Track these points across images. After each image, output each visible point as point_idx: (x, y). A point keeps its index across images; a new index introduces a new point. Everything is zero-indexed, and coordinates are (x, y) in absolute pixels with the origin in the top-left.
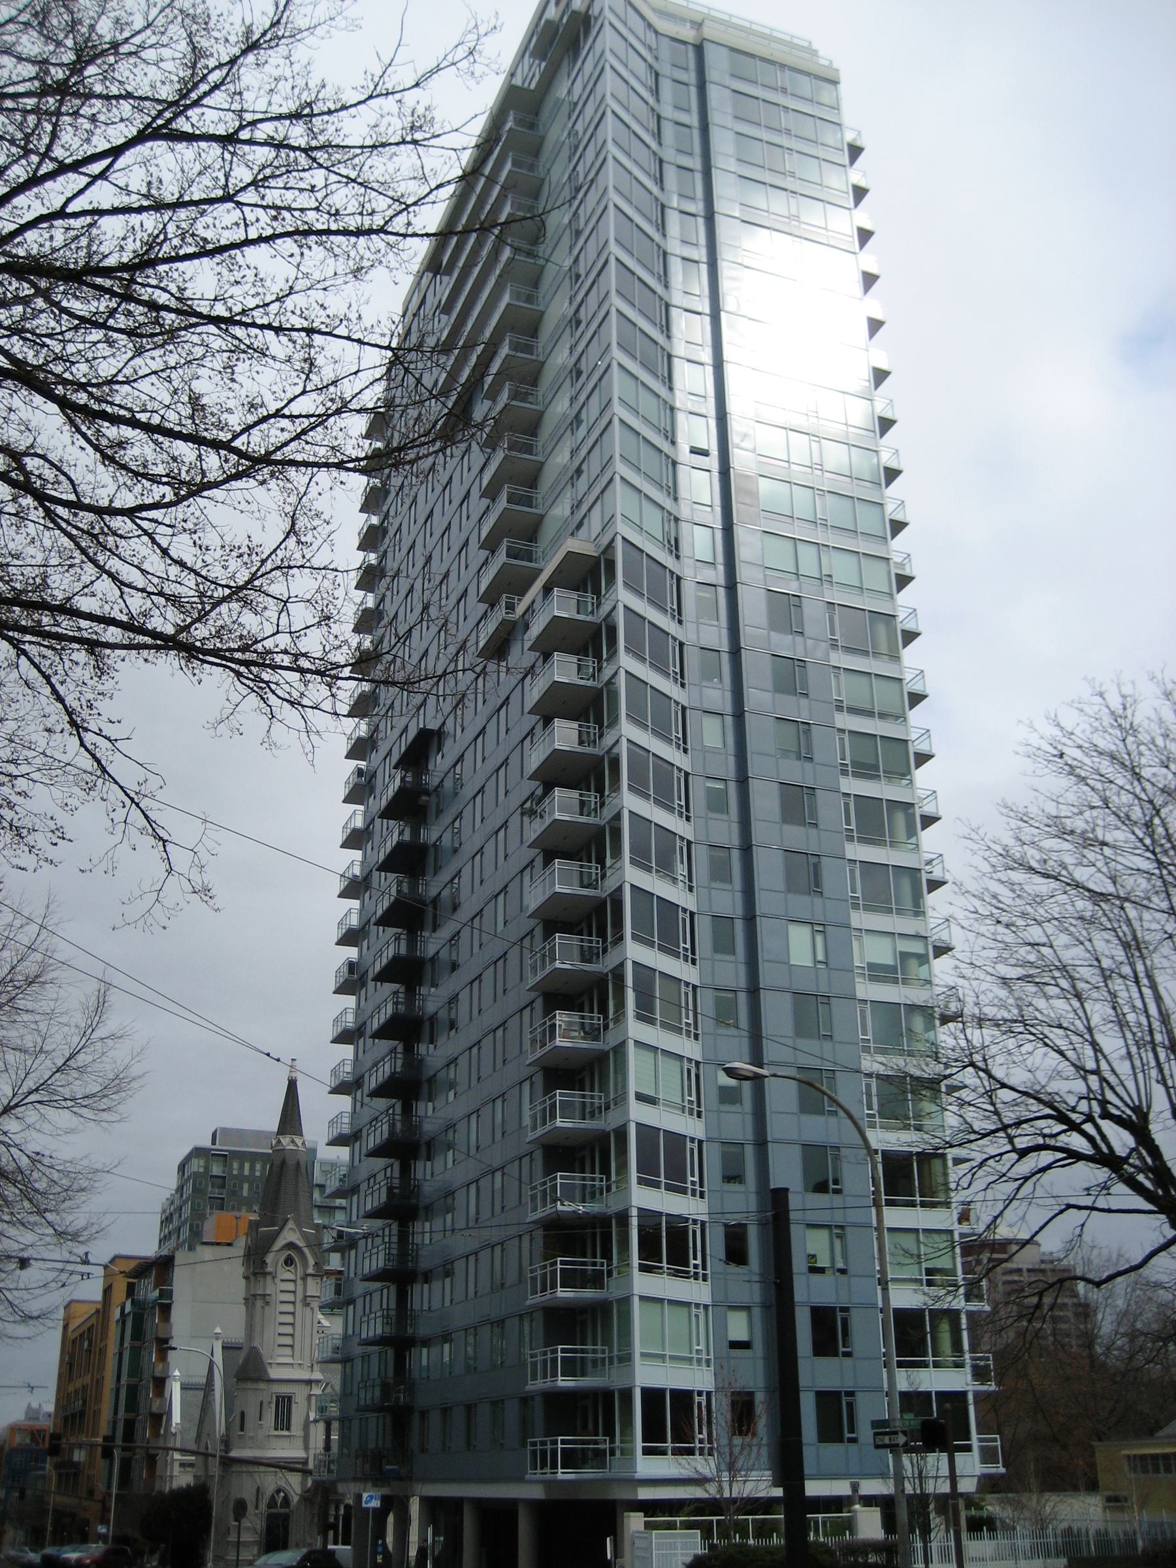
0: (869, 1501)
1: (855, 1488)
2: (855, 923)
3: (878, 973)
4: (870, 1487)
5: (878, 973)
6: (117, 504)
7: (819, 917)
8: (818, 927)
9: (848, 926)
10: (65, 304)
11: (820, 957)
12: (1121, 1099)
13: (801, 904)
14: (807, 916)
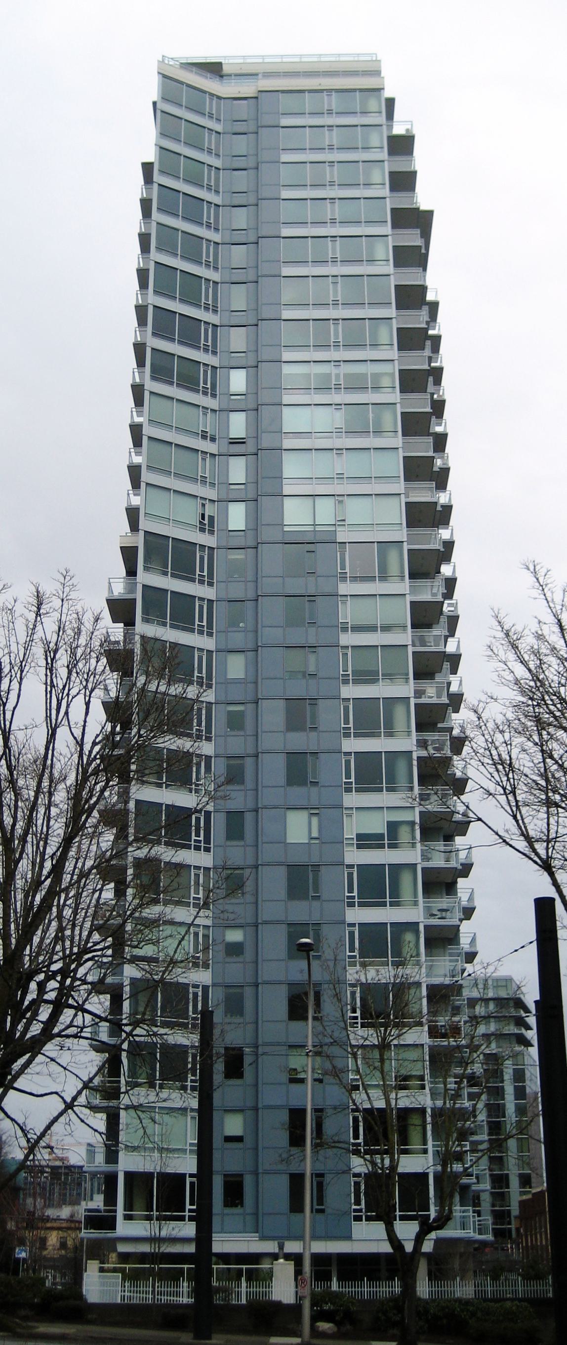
0: (288, 1257)
1: (281, 1247)
2: (346, 804)
3: (366, 841)
4: (292, 1247)
5: (366, 841)
6: (48, 848)
7: (314, 802)
8: (313, 810)
9: (341, 807)
10: (29, 838)
11: (315, 834)
12: (56, 720)
13: (297, 793)
14: (304, 803)
